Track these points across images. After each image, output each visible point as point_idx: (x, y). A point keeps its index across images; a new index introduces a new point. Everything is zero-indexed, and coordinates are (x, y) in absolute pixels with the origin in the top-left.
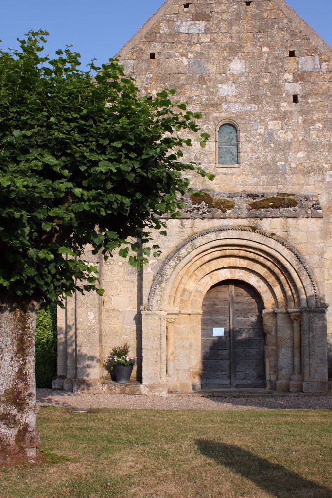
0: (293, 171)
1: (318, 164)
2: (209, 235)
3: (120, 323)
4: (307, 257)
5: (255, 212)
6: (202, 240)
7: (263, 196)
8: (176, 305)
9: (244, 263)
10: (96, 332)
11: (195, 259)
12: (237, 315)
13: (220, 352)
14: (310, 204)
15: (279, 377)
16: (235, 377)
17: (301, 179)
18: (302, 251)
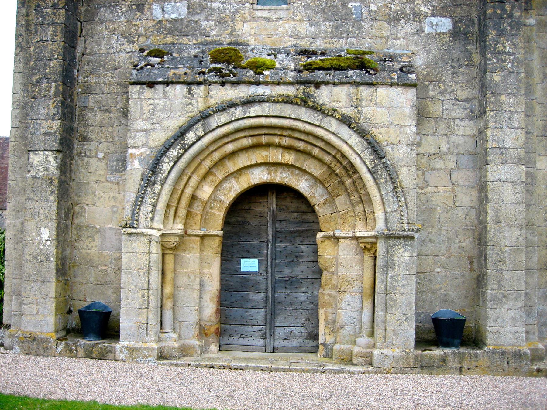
0: (373, 17)
1: (412, 5)
2: (232, 110)
3: (96, 246)
4: (388, 149)
5: (306, 74)
6: (220, 118)
7: (323, 54)
8: (178, 220)
9: (289, 158)
10: (52, 259)
11: (211, 149)
12: (280, 239)
13: (251, 296)
14: (398, 66)
15: (338, 339)
16: (273, 335)
17: (385, 29)
18: (380, 138)
